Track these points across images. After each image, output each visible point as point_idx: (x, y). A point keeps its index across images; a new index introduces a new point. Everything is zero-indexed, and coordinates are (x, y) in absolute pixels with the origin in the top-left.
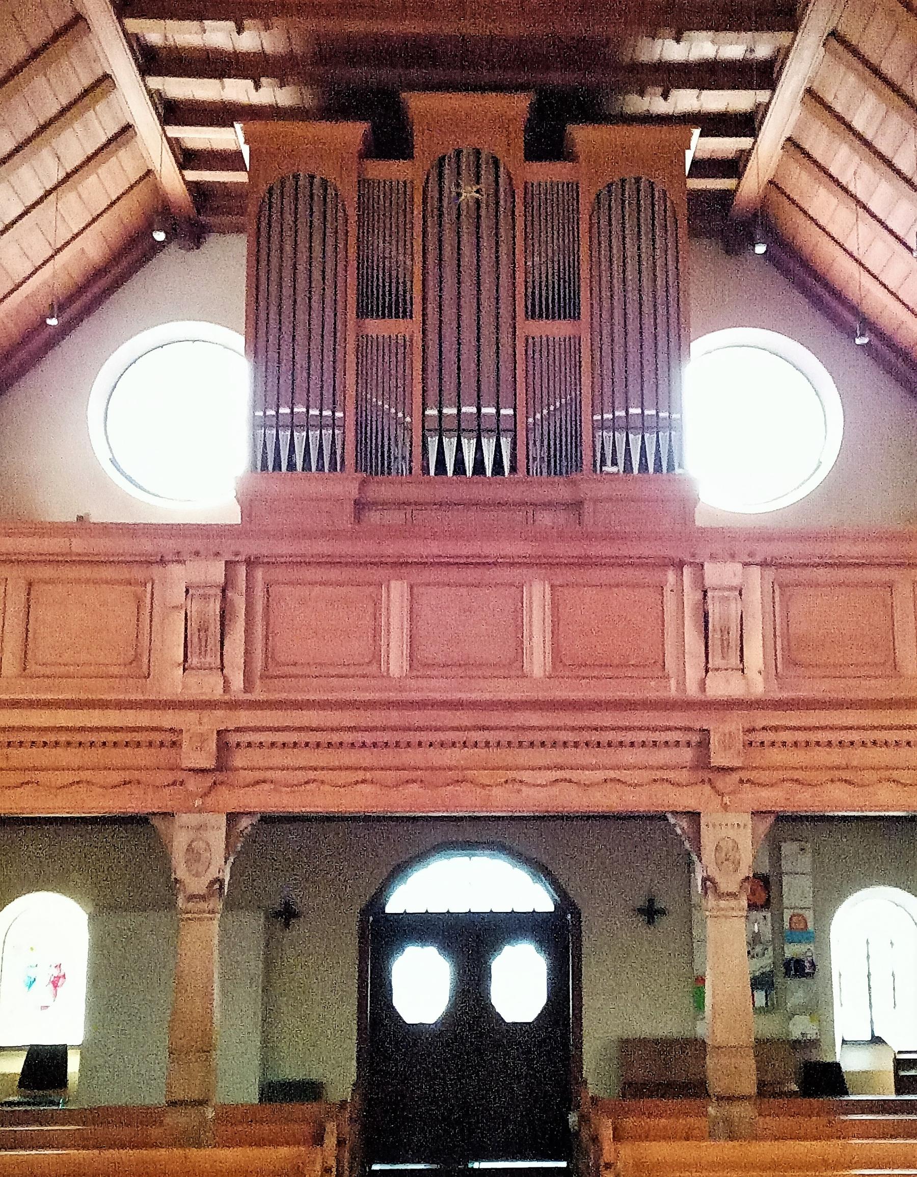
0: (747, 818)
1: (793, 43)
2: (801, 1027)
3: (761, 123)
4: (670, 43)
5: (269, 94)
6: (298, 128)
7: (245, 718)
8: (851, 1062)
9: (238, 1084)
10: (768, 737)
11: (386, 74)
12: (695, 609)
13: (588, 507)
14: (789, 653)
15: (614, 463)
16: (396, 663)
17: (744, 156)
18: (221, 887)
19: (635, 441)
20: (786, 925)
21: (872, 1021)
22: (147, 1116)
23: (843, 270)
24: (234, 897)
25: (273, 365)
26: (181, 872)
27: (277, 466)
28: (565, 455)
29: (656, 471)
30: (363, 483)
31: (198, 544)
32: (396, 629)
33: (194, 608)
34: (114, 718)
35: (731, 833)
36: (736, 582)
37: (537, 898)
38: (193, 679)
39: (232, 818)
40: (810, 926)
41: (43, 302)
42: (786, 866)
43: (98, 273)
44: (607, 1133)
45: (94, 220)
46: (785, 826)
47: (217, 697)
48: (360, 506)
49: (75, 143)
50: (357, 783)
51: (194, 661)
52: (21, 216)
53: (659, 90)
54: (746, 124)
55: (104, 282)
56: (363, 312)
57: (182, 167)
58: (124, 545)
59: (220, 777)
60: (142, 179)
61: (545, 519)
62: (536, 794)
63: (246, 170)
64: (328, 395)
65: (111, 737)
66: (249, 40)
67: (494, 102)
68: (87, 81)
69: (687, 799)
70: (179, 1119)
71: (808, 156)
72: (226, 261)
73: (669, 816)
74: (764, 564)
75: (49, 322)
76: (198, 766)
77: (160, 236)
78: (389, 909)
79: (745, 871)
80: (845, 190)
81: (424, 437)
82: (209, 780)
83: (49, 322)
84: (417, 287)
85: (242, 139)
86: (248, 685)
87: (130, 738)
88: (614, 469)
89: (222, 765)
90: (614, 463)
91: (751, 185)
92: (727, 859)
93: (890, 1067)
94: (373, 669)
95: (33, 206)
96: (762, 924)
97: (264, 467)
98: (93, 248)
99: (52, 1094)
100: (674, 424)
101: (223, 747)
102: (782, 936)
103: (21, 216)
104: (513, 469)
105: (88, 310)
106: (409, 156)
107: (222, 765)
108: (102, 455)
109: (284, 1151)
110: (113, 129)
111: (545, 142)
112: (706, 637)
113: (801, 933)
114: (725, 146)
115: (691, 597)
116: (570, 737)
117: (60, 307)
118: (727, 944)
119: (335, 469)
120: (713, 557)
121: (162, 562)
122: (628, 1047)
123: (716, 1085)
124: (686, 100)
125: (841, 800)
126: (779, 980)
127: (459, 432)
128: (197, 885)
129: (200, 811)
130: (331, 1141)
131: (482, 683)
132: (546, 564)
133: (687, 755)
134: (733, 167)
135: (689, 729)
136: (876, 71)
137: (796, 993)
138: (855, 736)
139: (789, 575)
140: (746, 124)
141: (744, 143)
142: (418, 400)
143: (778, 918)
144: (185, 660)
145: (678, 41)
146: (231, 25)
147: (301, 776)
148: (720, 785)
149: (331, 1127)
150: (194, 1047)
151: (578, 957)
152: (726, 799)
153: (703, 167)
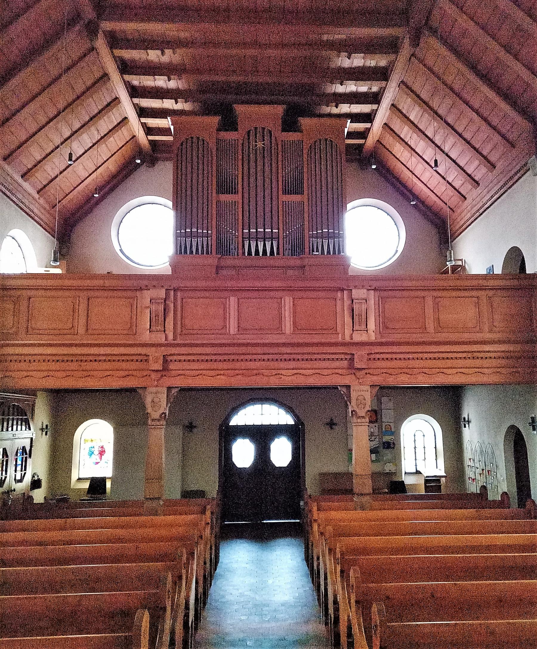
0: (368, 388)
1: (387, 85)
2: (389, 468)
3: (374, 117)
4: (339, 85)
5: (180, 106)
6: (190, 119)
7: (173, 350)
8: (408, 481)
9: (174, 493)
10: (378, 356)
12: (349, 308)
13: (307, 268)
14: (384, 325)
15: (317, 251)
16: (233, 328)
17: (368, 130)
21: (416, 465)
22: (135, 504)
23: (406, 175)
24: (170, 420)
26: (149, 410)
28: (298, 248)
29: (333, 254)
31: (155, 283)
32: (232, 316)
33: (154, 307)
34: (122, 350)
35: (362, 393)
36: (364, 296)
37: (287, 419)
38: (153, 335)
39: (169, 389)
40: (393, 430)
41: (92, 187)
42: (383, 406)
43: (114, 177)
44: (315, 508)
45: (112, 155)
46: (383, 391)
48: (218, 268)
49: (105, 124)
51: (153, 328)
52: (83, 154)
53: (334, 104)
54: (368, 118)
55: (115, 181)
56: (218, 193)
58: (129, 283)
59: (164, 373)
60: (131, 139)
61: (290, 272)
62: (289, 379)
63: (172, 136)
64: (268, 219)
65: (117, 358)
66: (172, 84)
67: (266, 109)
68: (109, 100)
69: (346, 381)
70: (148, 504)
71: (392, 130)
72: (165, 172)
73: (339, 387)
74: (375, 290)
75: (95, 195)
76: (156, 369)
77: (138, 161)
78: (230, 424)
79: (368, 408)
80: (406, 143)
81: (243, 241)
82: (159, 375)
83: (95, 195)
85: (170, 123)
88: (318, 253)
89: (165, 369)
90: (317, 251)
91: (370, 141)
94: (223, 331)
95: (89, 149)
96: (375, 429)
98: (112, 166)
99: (101, 496)
100: (341, 235)
102: (382, 433)
103: (83, 154)
104: (278, 253)
105: (112, 190)
106: (236, 130)
107: (165, 369)
108: (117, 249)
109: (193, 516)
110: (120, 120)
111: (290, 124)
112: (353, 319)
114: (360, 126)
115: (347, 303)
117: (99, 189)
118: (361, 437)
119: (209, 254)
120: (355, 287)
121: (141, 289)
122: (324, 476)
123: (356, 490)
124: (345, 108)
125: (404, 380)
128: (156, 415)
129: (157, 386)
130: (208, 513)
132: (289, 290)
134: (363, 135)
135: (346, 354)
136: (418, 96)
137: (388, 454)
138: (411, 356)
139: (386, 294)
140: (368, 118)
141: (368, 125)
142: (240, 227)
144: (150, 328)
145: (342, 85)
146: (166, 78)
148: (357, 374)
149: (208, 507)
150: (155, 477)
151: (304, 441)
152: (361, 381)
153: (351, 135)
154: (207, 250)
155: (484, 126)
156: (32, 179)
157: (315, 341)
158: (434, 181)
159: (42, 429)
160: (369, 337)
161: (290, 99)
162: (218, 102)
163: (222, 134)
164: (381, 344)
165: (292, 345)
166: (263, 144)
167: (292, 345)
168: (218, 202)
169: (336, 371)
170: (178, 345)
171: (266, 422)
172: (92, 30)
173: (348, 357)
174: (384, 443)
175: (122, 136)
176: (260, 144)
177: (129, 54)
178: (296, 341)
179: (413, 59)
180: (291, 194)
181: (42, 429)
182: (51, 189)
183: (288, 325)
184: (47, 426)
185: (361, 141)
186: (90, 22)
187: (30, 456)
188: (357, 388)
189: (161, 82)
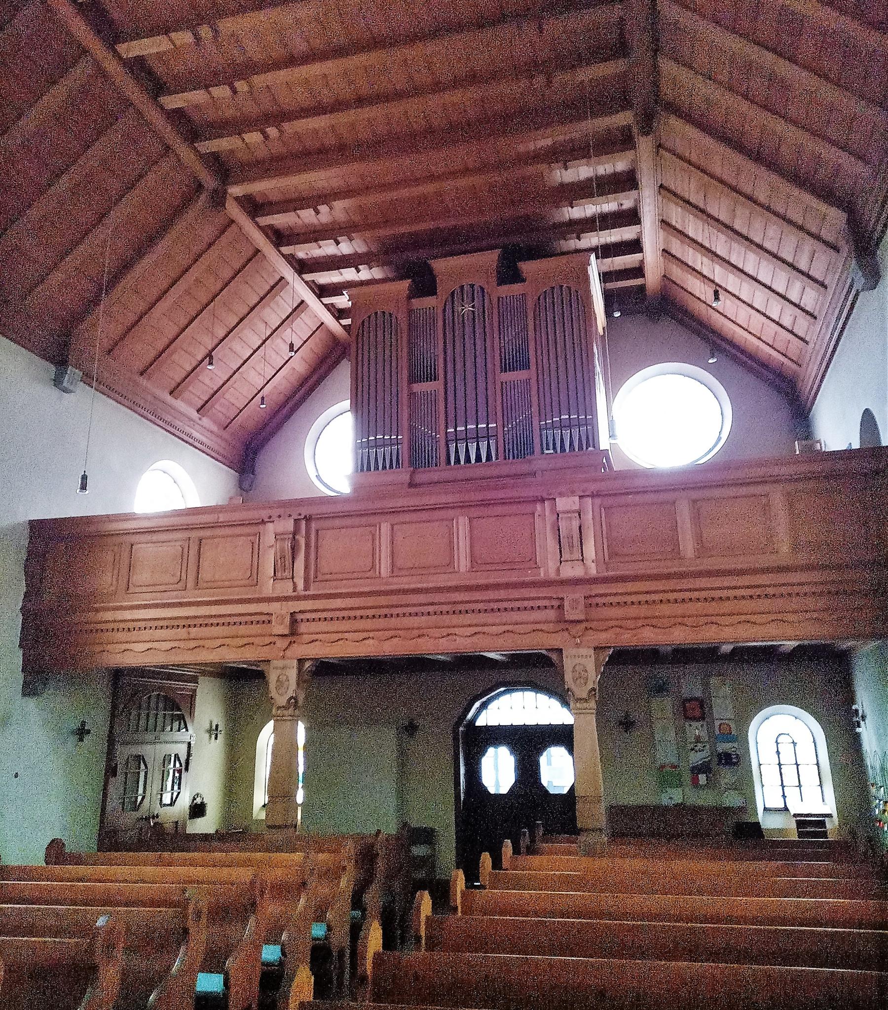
2: (732, 800)
5: (365, 274)
6: (387, 286)
8: (769, 823)
11: (423, 254)
12: (553, 527)
16: (385, 568)
18: (296, 702)
19: (575, 432)
20: (717, 732)
25: (365, 414)
26: (273, 693)
27: (369, 469)
30: (413, 472)
36: (576, 507)
38: (280, 585)
39: (301, 661)
47: (289, 594)
50: (364, 639)
51: (279, 575)
57: (338, 319)
69: (555, 641)
71: (673, 256)
74: (592, 496)
78: (477, 724)
82: (289, 639)
84: (441, 360)
86: (306, 588)
87: (249, 619)
92: (581, 677)
93: (794, 826)
97: (362, 470)
98: (299, 365)
101: (294, 622)
107: (294, 632)
111: (509, 273)
113: (728, 737)
115: (550, 518)
116: (480, 606)
120: (561, 495)
121: (263, 522)
126: (714, 766)
127: (477, 439)
128: (282, 701)
131: (431, 578)
132: (463, 506)
133: (551, 614)
135: (551, 598)
136: (688, 202)
137: (726, 776)
139: (610, 501)
141: (638, 256)
142: (443, 427)
143: (711, 725)
147: (336, 637)
154: (398, 461)
155: (787, 228)
156: (186, 395)
157: (491, 581)
158: (757, 322)
159: (210, 731)
160: (586, 568)
161: (504, 240)
162: (412, 261)
163: (416, 303)
164: (605, 580)
165: (469, 588)
166: (473, 307)
167: (469, 588)
168: (412, 395)
169: (538, 626)
170: (306, 598)
171: (531, 721)
172: (218, 200)
173: (556, 603)
174: (719, 755)
175: (303, 325)
176: (468, 308)
177: (280, 220)
178: (473, 582)
179: (662, 151)
180: (506, 371)
181: (210, 731)
182: (218, 408)
183: (462, 559)
184: (217, 726)
185: (638, 282)
186: (215, 191)
187: (187, 769)
188: (574, 651)
189: (328, 248)
